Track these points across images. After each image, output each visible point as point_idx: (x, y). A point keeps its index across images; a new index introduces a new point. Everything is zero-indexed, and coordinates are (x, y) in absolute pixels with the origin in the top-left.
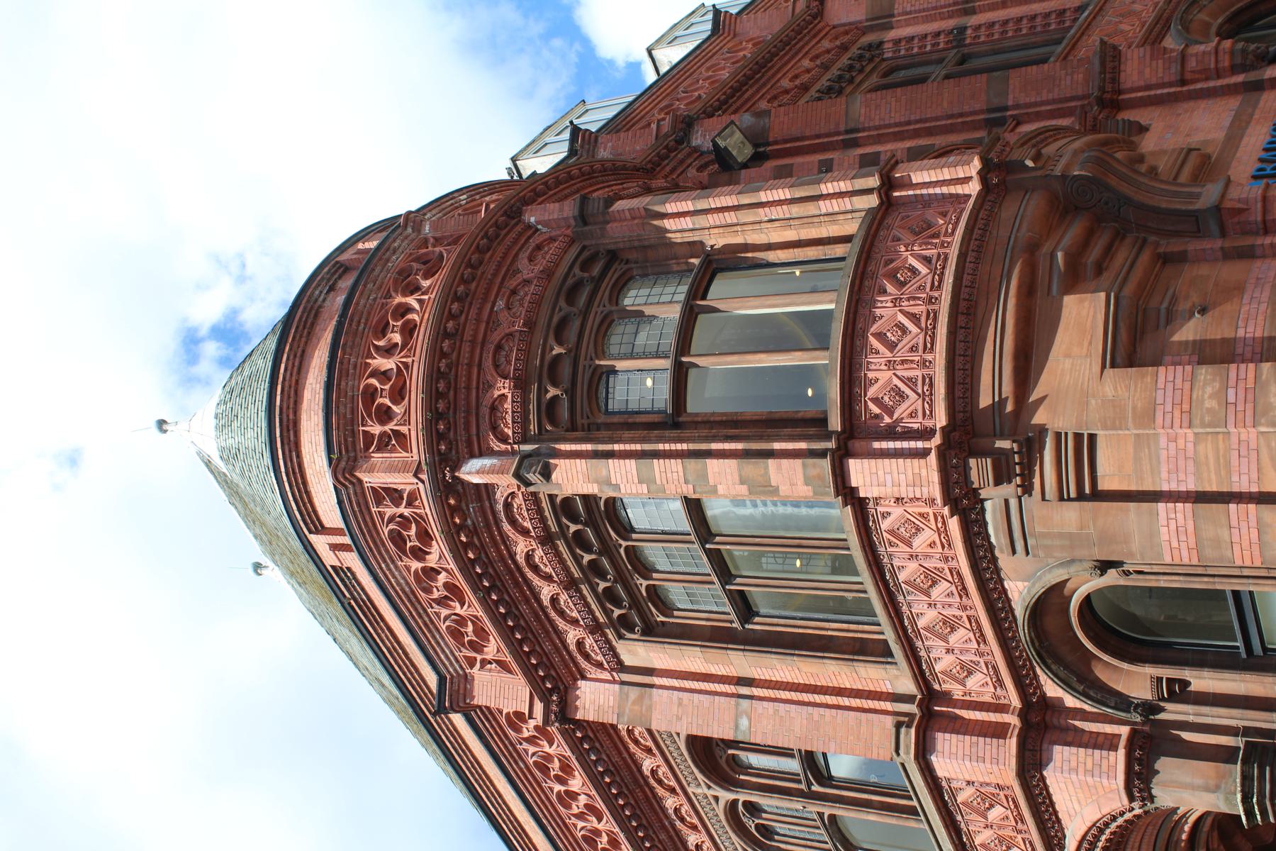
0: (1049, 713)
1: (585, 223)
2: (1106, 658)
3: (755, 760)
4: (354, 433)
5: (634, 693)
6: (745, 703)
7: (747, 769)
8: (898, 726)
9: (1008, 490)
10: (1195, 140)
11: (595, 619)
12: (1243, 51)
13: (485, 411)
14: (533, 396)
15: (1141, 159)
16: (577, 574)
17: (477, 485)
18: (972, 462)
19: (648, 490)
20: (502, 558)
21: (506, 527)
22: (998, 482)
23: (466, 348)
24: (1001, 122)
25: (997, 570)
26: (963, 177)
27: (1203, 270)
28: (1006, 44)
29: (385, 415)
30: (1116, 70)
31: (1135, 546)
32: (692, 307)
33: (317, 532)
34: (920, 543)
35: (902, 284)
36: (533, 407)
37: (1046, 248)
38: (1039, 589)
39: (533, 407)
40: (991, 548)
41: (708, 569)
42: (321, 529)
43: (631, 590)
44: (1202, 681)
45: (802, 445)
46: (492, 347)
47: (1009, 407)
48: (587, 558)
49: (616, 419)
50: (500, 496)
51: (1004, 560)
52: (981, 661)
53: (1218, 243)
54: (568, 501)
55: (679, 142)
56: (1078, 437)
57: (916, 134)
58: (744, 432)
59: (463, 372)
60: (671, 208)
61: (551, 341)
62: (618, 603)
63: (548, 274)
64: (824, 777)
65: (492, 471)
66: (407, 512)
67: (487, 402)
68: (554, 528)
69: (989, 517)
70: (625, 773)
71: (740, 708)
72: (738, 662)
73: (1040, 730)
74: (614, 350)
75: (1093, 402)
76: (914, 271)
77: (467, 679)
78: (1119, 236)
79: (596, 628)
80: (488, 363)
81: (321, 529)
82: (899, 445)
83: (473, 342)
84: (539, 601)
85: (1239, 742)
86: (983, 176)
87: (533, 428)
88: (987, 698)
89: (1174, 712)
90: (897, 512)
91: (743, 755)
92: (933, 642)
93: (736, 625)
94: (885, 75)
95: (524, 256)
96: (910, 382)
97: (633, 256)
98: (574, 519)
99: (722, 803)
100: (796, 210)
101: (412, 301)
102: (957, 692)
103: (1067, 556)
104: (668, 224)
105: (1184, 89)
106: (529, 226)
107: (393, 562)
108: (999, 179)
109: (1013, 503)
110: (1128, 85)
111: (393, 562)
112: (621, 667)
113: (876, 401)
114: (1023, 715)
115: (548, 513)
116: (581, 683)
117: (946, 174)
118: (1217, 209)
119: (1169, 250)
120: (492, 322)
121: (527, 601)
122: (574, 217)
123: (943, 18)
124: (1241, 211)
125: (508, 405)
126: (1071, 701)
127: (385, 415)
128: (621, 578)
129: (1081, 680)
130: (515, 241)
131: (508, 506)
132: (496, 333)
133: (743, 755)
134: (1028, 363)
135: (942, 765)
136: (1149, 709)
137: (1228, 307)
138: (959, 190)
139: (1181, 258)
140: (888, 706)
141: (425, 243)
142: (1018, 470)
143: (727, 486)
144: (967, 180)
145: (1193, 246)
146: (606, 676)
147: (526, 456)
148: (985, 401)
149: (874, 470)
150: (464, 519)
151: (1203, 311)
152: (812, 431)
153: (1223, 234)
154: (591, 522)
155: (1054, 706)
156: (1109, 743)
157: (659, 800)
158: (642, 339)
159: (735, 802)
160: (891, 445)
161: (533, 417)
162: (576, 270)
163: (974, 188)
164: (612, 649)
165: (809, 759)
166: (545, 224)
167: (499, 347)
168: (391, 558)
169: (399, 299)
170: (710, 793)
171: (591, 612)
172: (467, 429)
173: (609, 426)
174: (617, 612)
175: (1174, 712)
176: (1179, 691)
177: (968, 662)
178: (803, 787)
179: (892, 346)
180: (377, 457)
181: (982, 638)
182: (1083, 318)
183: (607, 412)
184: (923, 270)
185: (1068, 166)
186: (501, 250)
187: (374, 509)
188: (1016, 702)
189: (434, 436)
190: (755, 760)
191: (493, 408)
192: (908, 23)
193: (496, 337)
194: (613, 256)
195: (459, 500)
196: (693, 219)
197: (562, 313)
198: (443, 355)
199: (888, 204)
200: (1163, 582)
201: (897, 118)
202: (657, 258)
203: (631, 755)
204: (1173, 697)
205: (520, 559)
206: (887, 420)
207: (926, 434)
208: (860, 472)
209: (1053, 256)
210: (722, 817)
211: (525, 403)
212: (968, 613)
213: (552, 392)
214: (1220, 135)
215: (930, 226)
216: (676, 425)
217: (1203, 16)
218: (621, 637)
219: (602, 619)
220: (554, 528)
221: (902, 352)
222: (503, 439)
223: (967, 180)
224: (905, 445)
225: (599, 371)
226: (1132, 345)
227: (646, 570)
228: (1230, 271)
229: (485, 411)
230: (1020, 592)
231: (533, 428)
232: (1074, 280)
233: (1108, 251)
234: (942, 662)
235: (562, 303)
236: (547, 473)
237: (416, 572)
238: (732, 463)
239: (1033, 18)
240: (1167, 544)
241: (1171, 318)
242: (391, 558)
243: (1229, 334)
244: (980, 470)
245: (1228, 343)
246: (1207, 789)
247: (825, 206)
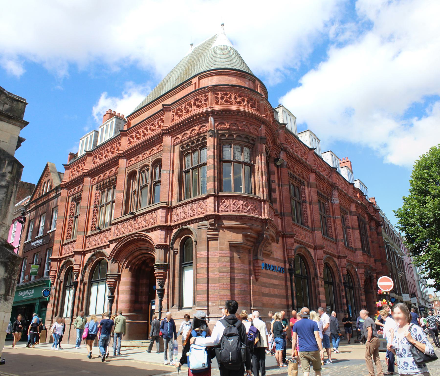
1: (261, 139)
2: (181, 240)
3: (158, 170)
4: (218, 91)
5: (169, 149)
6: (169, 172)
7: (156, 169)
8: (166, 203)
9: (208, 226)
10: (275, 253)
11: (183, 142)
12: (292, 260)
13: (223, 122)
14: (226, 132)
15: (270, 244)
16: (192, 139)
17: (208, 120)
18: (213, 220)
19: (208, 154)
20: (194, 124)
21: (200, 125)
22: (210, 224)
23: (235, 117)
24: (281, 216)
25: (195, 223)
26: (265, 216)
27: (247, 257)
28: (302, 212)
29: (222, 98)
30: (290, 237)
31: (199, 247)
33: (199, 79)
34: (199, 209)
35: (245, 205)
36: (224, 132)
37: (251, 231)
38: (192, 230)
39: (224, 132)
40: (199, 222)
41: (194, 166)
43: (189, 149)
44: (178, 257)
45: (216, 188)
46: (235, 122)
47: (223, 226)
48: (195, 141)
49: (222, 148)
50: (206, 124)
51: (197, 224)
53: (252, 259)
54: (205, 138)
55: (282, 149)
56: (218, 238)
57: (280, 199)
58: (219, 176)
59: (230, 117)
60: (263, 157)
61: (237, 135)
62: (187, 146)
64: (155, 185)
65: (211, 124)
66: (203, 102)
67: (225, 122)
68: (201, 135)
69: (204, 222)
72: (176, 171)
73: (168, 229)
74: (235, 147)
76: (248, 207)
77: (170, 111)
78: (254, 242)
79: (182, 142)
80: (232, 122)
81: (199, 79)
82: (216, 206)
84: (186, 130)
85: (167, 263)
86: (265, 219)
87: (220, 132)
88: (172, 219)
89: (172, 252)
90: (205, 205)
91: (158, 168)
92: (182, 210)
93: (183, 170)
94: (297, 187)
95: (254, 126)
96: (227, 208)
98: (202, 140)
99: (148, 164)
100: (261, 183)
101: (246, 103)
102: (173, 213)
103: (198, 235)
104: (260, 157)
105: (285, 249)
106: (261, 126)
108: (265, 222)
110: (287, 239)
112: (174, 146)
113: (224, 201)
114: (170, 226)
115: (204, 134)
116: (171, 137)
117: (266, 212)
118: (258, 259)
120: (240, 122)
121: (186, 128)
123: (309, 198)
124: (257, 263)
125: (224, 126)
126: (173, 234)
127: (222, 98)
128: (191, 148)
129: (176, 236)
130: (257, 124)
131: (205, 126)
133: (158, 168)
134: (230, 229)
135: (160, 211)
136: (172, 248)
137: (240, 262)
138: (263, 214)
139: (249, 253)
140: (170, 200)
141: (258, 102)
142: (212, 227)
143: (209, 172)
144: (264, 216)
145: (251, 255)
146: (172, 143)
147: (214, 131)
148: (224, 221)
151: (239, 258)
152: (219, 189)
153: (253, 260)
155: (172, 231)
156: (166, 241)
157: (148, 150)
158: (237, 153)
159: (149, 166)
160: (216, 205)
161: (222, 132)
162: (251, 138)
163: (263, 217)
164: (178, 144)
165: (159, 182)
166: (261, 130)
167: (236, 124)
169: (246, 99)
170: (150, 161)
171: (185, 141)
172: (219, 118)
173: (220, 147)
174: (185, 146)
175: (172, 252)
176: (175, 253)
177: (179, 216)
178: (153, 181)
179: (234, 204)
180: (214, 96)
182: (238, 238)
184: (248, 209)
185: (266, 234)
186: (255, 122)
187: (203, 95)
188: (172, 224)
190: (158, 170)
191: (223, 123)
192: (308, 191)
193: (238, 123)
194: (254, 145)
196: (260, 162)
198: (234, 113)
199: (261, 201)
200: (194, 251)
201: (283, 195)
202: (253, 155)
203: (157, 145)
204: (174, 252)
205: (194, 128)
206: (221, 204)
207: (218, 212)
208: (211, 199)
209: (249, 232)
210: (146, 163)
211: (224, 130)
213: (227, 136)
214: (275, 257)
215: (256, 209)
216: (220, 161)
217: (303, 250)
218: (180, 146)
219: (184, 143)
220: (201, 135)
221: (233, 206)
222: (217, 126)
223: (264, 216)
224: (216, 207)
226: (233, 246)
227: (193, 152)
228: (247, 261)
229: (223, 122)
230: (191, 227)
231: (220, 132)
232: (245, 236)
233: (250, 241)
234: (179, 211)
235: (244, 136)
236: (211, 136)
238: (213, 174)
239: (307, 217)
240: (200, 252)
241: (238, 252)
243: (235, 262)
244: (212, 221)
245: (234, 262)
246: (159, 258)
247: (261, 189)
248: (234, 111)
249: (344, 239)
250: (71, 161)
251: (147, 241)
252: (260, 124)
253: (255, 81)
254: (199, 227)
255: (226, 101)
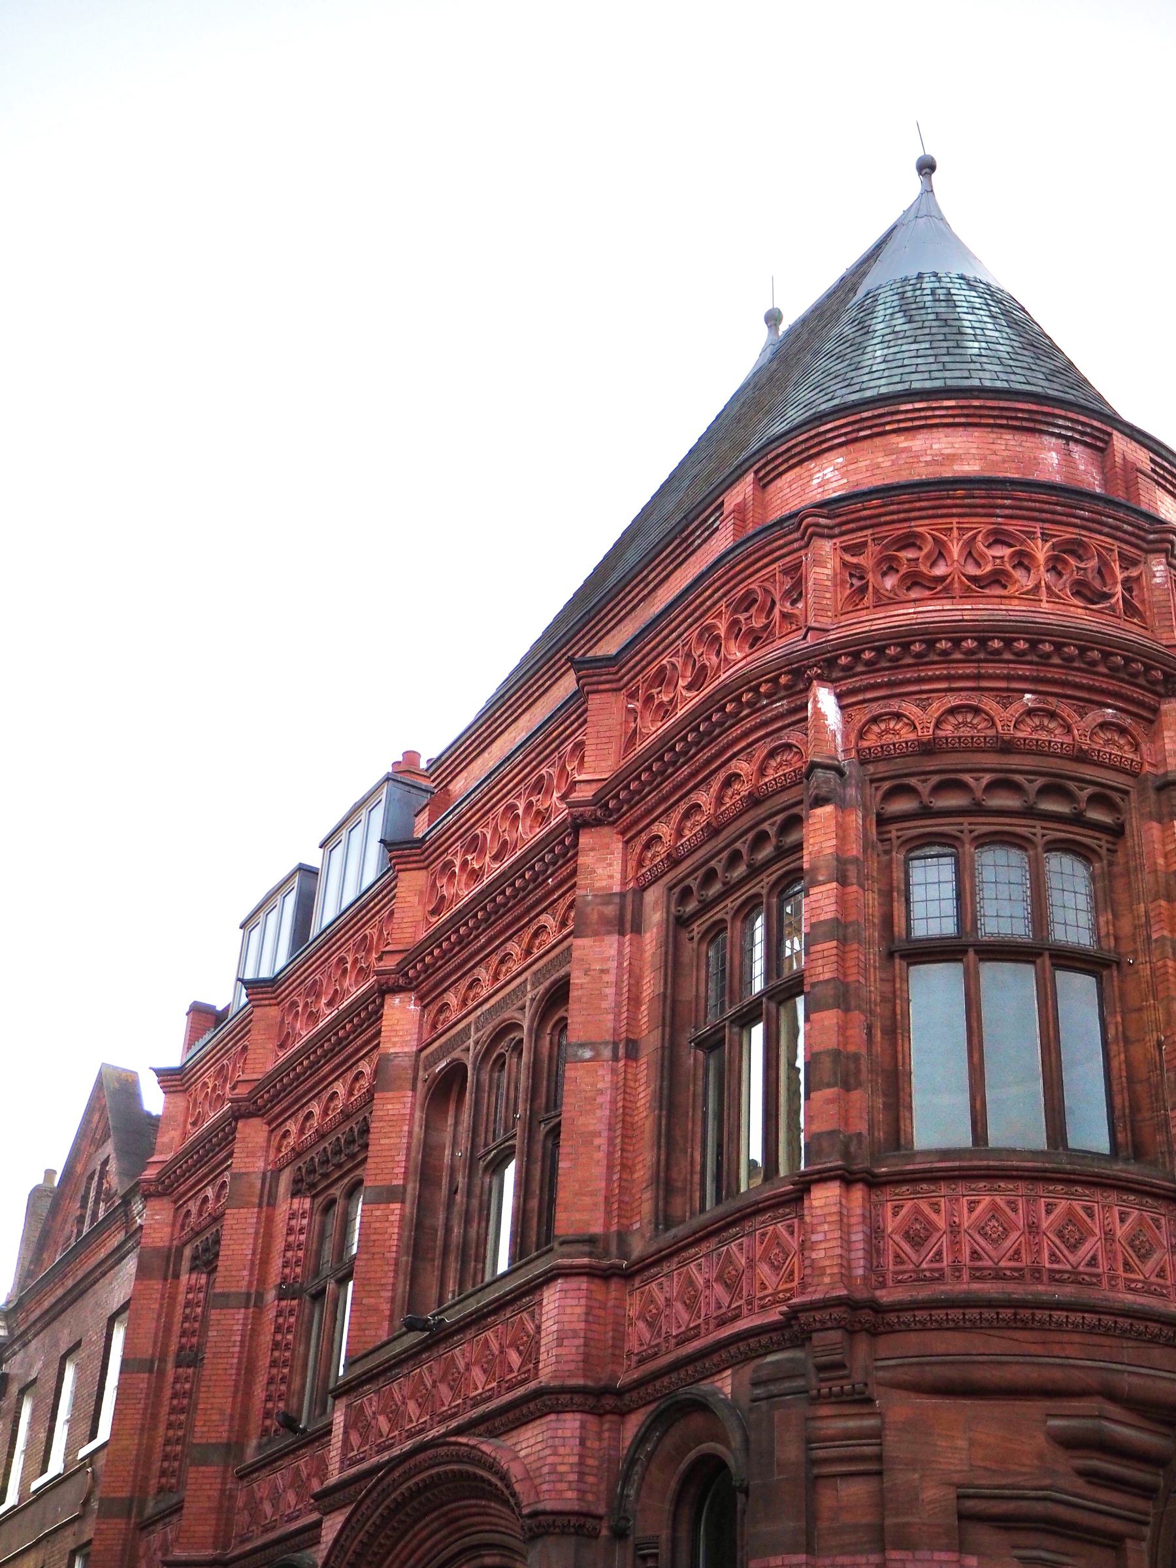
0: (615, 1418)
32: (1040, 955)
42: (763, 484)
49: (898, 874)
52: (662, 1339)
63: (1082, 757)
70: (539, 893)
71: (602, 1047)
75: (916, 1476)
79: (673, 861)
81: (763, 484)
83: (978, 677)
97: (1120, 858)
99: (517, 1015)
107: (725, 595)
109: (799, 1383)
111: (725, 595)
119: (1130, 1554)
122: (1166, 774)
132: (995, 705)
149: (829, 1219)
150: (768, 696)
154: (782, 853)
159: (520, 1027)
162: (1090, 790)
164: (657, 879)
167: (976, 711)
168: (729, 591)
181: (682, 1340)
183: (907, 860)
189: (854, 647)
194: (1117, 832)
195: (787, 687)
197: (1026, 784)
212: (703, 1326)
225: (957, 844)
235: (1040, 781)
237: (714, 626)
242: (729, 591)
248: (956, 633)
249: (918, 1364)
250: (195, 1049)
251: (484, 1486)
252: (1149, 698)
253: (1107, 439)
254: (758, 1391)
255: (914, 580)
